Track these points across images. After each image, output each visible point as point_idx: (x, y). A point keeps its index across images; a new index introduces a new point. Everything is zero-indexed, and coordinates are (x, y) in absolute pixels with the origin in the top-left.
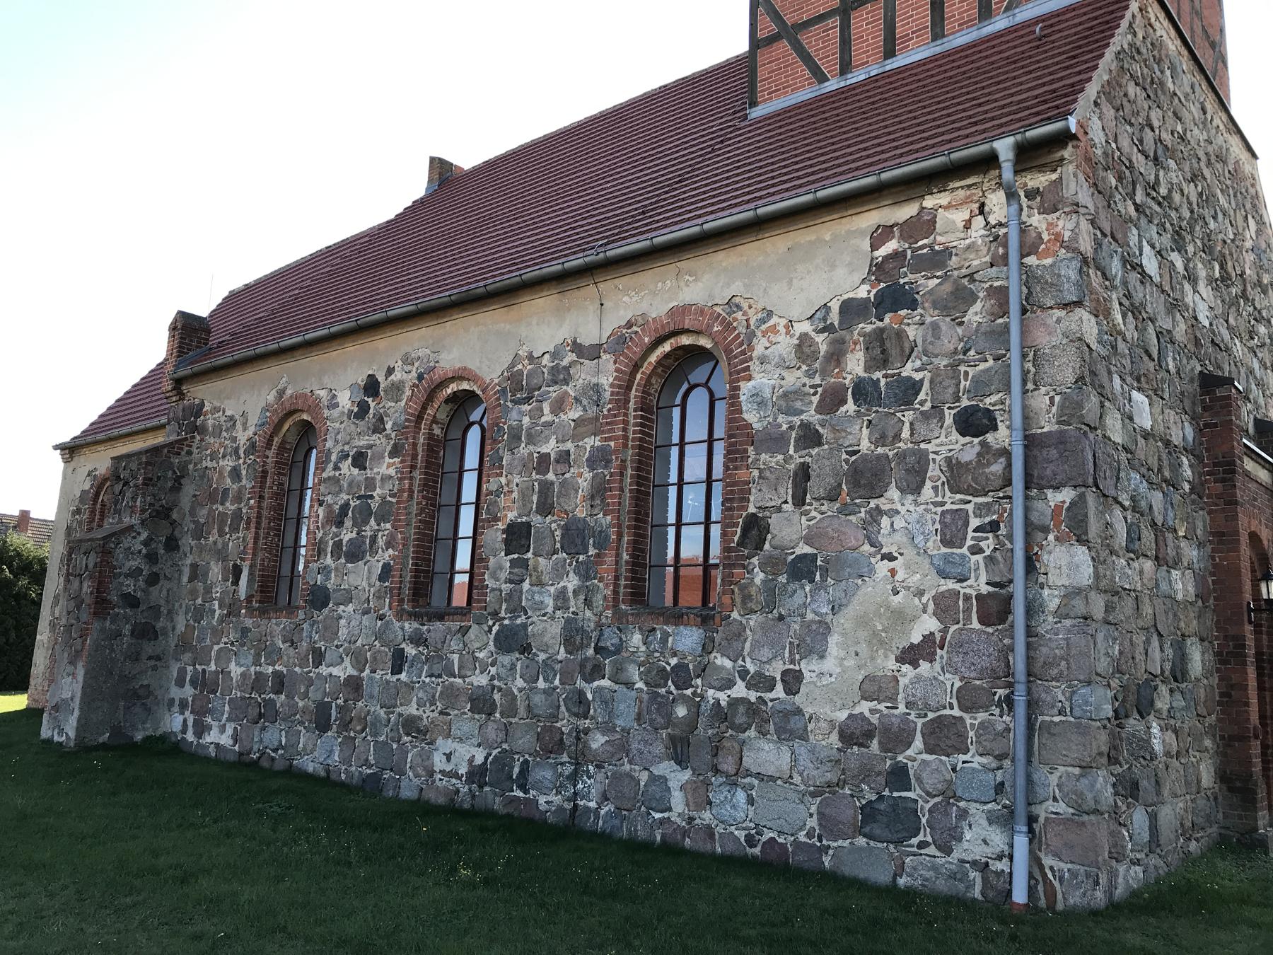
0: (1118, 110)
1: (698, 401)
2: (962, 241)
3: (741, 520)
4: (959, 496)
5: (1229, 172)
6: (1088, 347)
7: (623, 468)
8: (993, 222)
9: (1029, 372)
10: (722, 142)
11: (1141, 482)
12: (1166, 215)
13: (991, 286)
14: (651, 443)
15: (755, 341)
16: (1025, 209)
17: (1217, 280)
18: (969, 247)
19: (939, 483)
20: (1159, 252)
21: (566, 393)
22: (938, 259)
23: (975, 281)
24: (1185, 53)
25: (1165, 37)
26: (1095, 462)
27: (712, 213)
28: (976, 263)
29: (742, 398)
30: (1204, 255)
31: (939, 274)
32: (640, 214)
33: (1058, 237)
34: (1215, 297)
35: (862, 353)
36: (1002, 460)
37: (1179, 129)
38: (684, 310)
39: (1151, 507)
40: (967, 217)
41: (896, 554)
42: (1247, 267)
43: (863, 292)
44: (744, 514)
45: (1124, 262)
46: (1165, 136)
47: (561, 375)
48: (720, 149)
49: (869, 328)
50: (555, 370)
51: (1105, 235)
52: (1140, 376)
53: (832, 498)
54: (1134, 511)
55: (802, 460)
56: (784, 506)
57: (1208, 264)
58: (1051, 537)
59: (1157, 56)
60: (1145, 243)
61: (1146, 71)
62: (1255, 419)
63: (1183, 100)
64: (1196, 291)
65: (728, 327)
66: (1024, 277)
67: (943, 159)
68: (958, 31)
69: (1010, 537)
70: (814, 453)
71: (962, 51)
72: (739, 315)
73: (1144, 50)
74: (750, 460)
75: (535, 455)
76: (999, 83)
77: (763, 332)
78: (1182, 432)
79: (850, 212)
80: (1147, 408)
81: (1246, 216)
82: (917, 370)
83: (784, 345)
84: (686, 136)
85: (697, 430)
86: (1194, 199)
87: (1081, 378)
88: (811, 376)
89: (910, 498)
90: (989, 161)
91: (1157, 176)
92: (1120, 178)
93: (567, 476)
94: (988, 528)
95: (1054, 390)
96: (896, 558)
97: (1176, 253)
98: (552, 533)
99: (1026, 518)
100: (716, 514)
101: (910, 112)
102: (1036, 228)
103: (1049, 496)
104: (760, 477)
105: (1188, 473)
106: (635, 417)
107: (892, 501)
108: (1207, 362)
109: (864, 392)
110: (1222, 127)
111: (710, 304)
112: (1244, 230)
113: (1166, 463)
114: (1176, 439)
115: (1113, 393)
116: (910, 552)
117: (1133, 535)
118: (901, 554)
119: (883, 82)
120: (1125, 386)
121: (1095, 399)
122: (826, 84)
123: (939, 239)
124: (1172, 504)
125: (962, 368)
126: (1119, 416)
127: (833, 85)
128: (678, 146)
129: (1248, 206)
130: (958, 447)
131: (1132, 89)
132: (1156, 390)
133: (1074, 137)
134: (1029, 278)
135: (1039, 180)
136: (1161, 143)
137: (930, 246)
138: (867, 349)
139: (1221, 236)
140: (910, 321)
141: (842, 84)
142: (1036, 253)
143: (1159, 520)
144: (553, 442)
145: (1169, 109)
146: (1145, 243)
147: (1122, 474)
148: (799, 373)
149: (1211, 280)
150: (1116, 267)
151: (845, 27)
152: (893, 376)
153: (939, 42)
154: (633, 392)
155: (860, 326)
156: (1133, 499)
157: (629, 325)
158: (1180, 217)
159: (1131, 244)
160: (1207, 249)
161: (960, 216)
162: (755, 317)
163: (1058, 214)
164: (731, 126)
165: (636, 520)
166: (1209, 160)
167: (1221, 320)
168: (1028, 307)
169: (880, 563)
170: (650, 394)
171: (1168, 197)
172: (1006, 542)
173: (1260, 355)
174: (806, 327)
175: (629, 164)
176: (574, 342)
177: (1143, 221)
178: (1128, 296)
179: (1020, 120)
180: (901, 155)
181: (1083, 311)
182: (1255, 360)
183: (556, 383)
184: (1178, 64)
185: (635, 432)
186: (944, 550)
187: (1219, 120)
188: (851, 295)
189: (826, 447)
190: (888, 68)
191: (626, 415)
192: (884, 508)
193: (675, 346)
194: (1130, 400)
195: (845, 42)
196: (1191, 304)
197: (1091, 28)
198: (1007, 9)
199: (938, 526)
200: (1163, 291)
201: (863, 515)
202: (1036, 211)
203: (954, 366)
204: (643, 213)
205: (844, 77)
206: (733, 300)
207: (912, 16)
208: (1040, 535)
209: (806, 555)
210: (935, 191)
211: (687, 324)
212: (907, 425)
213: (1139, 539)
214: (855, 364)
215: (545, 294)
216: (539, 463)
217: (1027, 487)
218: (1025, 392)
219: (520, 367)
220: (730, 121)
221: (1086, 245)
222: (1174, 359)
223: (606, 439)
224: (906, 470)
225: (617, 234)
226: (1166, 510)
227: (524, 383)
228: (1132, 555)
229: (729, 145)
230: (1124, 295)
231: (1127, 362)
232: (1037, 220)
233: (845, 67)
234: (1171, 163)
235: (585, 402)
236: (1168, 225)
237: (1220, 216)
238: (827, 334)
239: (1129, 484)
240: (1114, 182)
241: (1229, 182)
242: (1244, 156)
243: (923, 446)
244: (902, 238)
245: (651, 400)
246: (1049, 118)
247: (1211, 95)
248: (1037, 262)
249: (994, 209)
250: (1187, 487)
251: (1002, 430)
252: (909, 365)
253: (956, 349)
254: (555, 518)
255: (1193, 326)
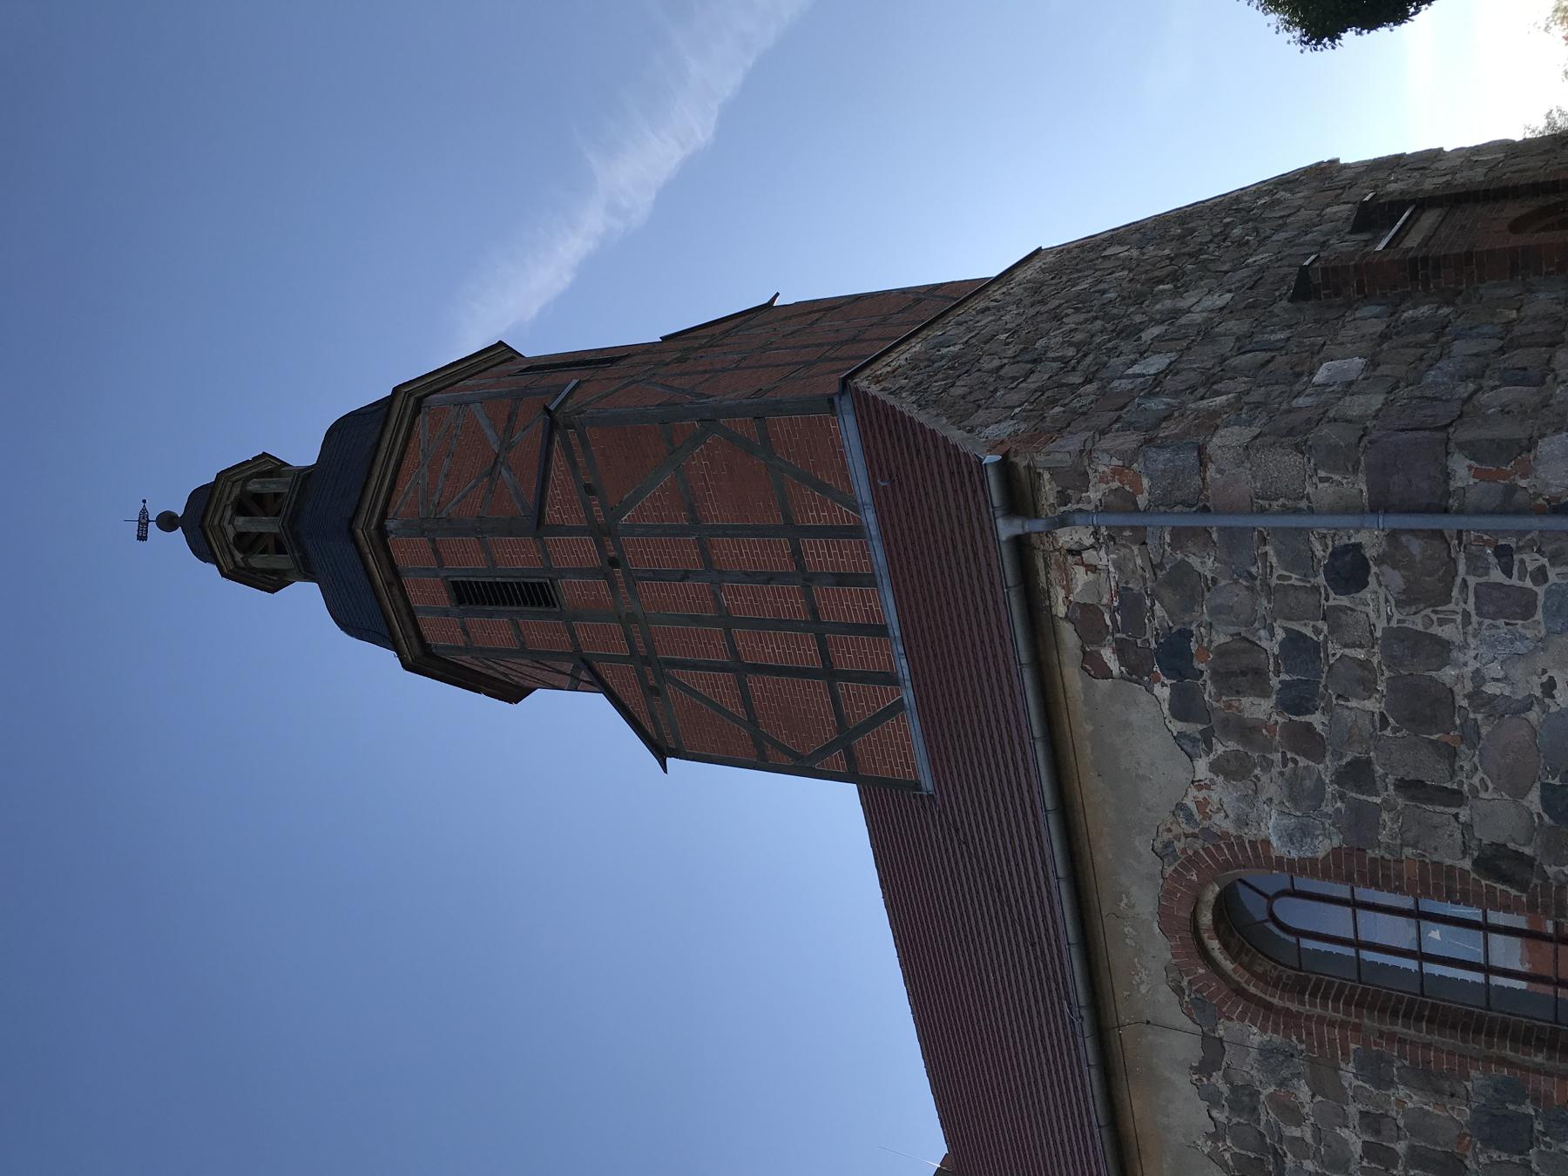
0: (979, 406)
1: (1294, 913)
2: (1111, 575)
3: (1483, 882)
4: (1455, 593)
5: (1052, 279)
6: (1256, 438)
7: (1391, 1038)
8: (1092, 540)
9: (1283, 505)
10: (957, 830)
11: (1439, 368)
12: (1099, 346)
13: (1169, 545)
14: (1353, 988)
15: (1215, 829)
16: (1080, 506)
17: (1175, 286)
18: (1118, 568)
19: (1434, 617)
20: (1141, 354)
21: (1271, 1097)
22: (1130, 604)
23: (1161, 563)
24: (925, 332)
25: (907, 355)
26: (1412, 430)
27: (1044, 863)
28: (1139, 561)
29: (1294, 855)
30: (1147, 303)
31: (1148, 603)
32: (1034, 950)
33: (1116, 472)
34: (1197, 288)
35: (1243, 700)
36: (1403, 539)
37: (1003, 337)
38: (1165, 915)
39: (1477, 355)
40: (1082, 569)
41: (1545, 679)
42: (1161, 253)
43: (1163, 692)
44: (1473, 875)
45: (1151, 394)
46: (1010, 353)
47: (1243, 1099)
48: (965, 834)
49: (1210, 687)
50: (1235, 1107)
51: (1118, 419)
52: (1294, 373)
53: (1453, 754)
54: (1482, 377)
55: (1391, 788)
56: (1462, 819)
57: (1157, 297)
58: (1523, 483)
59: (926, 363)
60: (1130, 371)
61: (940, 376)
62: (1351, 233)
63: (973, 334)
64: (1189, 311)
65: (1192, 861)
66: (1162, 508)
67: (1012, 594)
68: (870, 560)
69: (1521, 534)
70: (1381, 771)
71: (891, 557)
72: (1179, 846)
73: (919, 378)
74: (1387, 856)
75: (1365, 1163)
76: (933, 526)
77: (1204, 818)
78: (1369, 319)
79: (1062, 699)
80: (1336, 363)
81: (1102, 257)
82: (1272, 635)
83: (1223, 794)
84: (944, 869)
85: (1337, 921)
86: (1082, 317)
87: (1298, 448)
88: (1271, 763)
89: (1454, 654)
90: (1021, 545)
91: (1054, 360)
92: (1053, 402)
93: (1401, 1123)
94: (1504, 560)
95: (1310, 477)
96: (1551, 678)
97: (1143, 335)
98: (1493, 1163)
99: (1492, 513)
100: (1473, 913)
101: (939, 557)
102: (1104, 494)
103: (1460, 484)
104: (1415, 846)
105: (1425, 310)
106: (1313, 1005)
107: (1460, 678)
108: (1277, 294)
109: (1297, 700)
110: (1004, 290)
111: (1161, 881)
112: (1118, 259)
113: (1411, 339)
114: (1379, 326)
115: (1317, 407)
116: (1541, 660)
117: (1520, 377)
118: (1544, 672)
119: (910, 628)
120: (1308, 391)
121: (1325, 430)
122: (906, 702)
123: (1105, 601)
124: (1471, 329)
125: (1274, 582)
126: (1348, 399)
127: (908, 695)
128: (954, 883)
129: (1092, 255)
130: (1382, 592)
131: (957, 391)
132: (1312, 353)
133: (1005, 456)
134: (1163, 503)
135: (1049, 490)
136: (1018, 355)
137: (1113, 612)
138: (1238, 692)
139: (1125, 284)
140: (1206, 640)
141: (908, 684)
142: (1134, 495)
143: (1497, 344)
144: (1345, 1133)
145: (982, 348)
146: (1130, 371)
147: (1428, 393)
148: (1264, 779)
149: (1177, 293)
150: (1157, 405)
151: (848, 676)
152: (1277, 664)
153: (879, 580)
154: (1276, 1001)
155: (1206, 698)
156: (1465, 378)
157: (1179, 991)
158: (1102, 332)
159: (1130, 387)
160: (1139, 299)
161: (1081, 577)
162: (1183, 826)
163: (1090, 471)
164: (940, 816)
165: (1478, 1031)
166: (1039, 302)
167: (1225, 279)
168: (1201, 504)
169: (1559, 700)
170: (1279, 978)
171: (1078, 346)
172: (1528, 537)
173: (1269, 232)
174: (1202, 767)
175: (968, 946)
176: (1196, 1070)
177: (1104, 374)
178: (1192, 389)
179: (979, 510)
180: (1002, 637)
181: (1211, 444)
182: (1274, 238)
183: (1255, 1109)
184: (935, 341)
185: (1336, 1010)
186: (1539, 616)
187: (997, 293)
188: (1165, 707)
189: (1372, 754)
190: (897, 634)
191: (1309, 1018)
192: (1469, 687)
193: (1213, 934)
194: (1326, 385)
195: (864, 677)
196: (1205, 314)
197: (890, 433)
198: (856, 510)
199: (1501, 622)
200: (1188, 348)
201: (1479, 717)
202: (1084, 495)
203: (1270, 591)
204: (1033, 945)
205: (901, 682)
206: (1157, 851)
207: (848, 606)
208: (1519, 496)
209: (1542, 798)
210: (1047, 603)
211: (1185, 914)
212: (1347, 651)
213: (1525, 369)
214: (1258, 708)
215: (1126, 1097)
216: (1380, 1162)
217: (1446, 511)
218: (1311, 511)
219: (1227, 1156)
220: (933, 815)
221: (1130, 440)
222: (1273, 332)
223: (1345, 1053)
224: (1413, 656)
225: (1057, 984)
226: (1479, 335)
227: (1252, 1155)
228: (1549, 378)
229: (962, 822)
230: (1191, 393)
231: (1278, 389)
232: (1094, 494)
233: (891, 679)
234: (1040, 343)
235: (1285, 1073)
236: (1109, 345)
237: (1101, 286)
238: (1214, 740)
239: (1444, 384)
240: (1057, 409)
241: (1064, 279)
242: (1037, 263)
243: (1378, 634)
244: (1100, 642)
245: (1289, 977)
246: (982, 482)
247: (970, 304)
248: (1146, 494)
249: (1076, 539)
250: (1445, 310)
251: (1362, 537)
252: (1264, 644)
253: (1247, 588)
254: (1469, 1154)
255: (1231, 312)
